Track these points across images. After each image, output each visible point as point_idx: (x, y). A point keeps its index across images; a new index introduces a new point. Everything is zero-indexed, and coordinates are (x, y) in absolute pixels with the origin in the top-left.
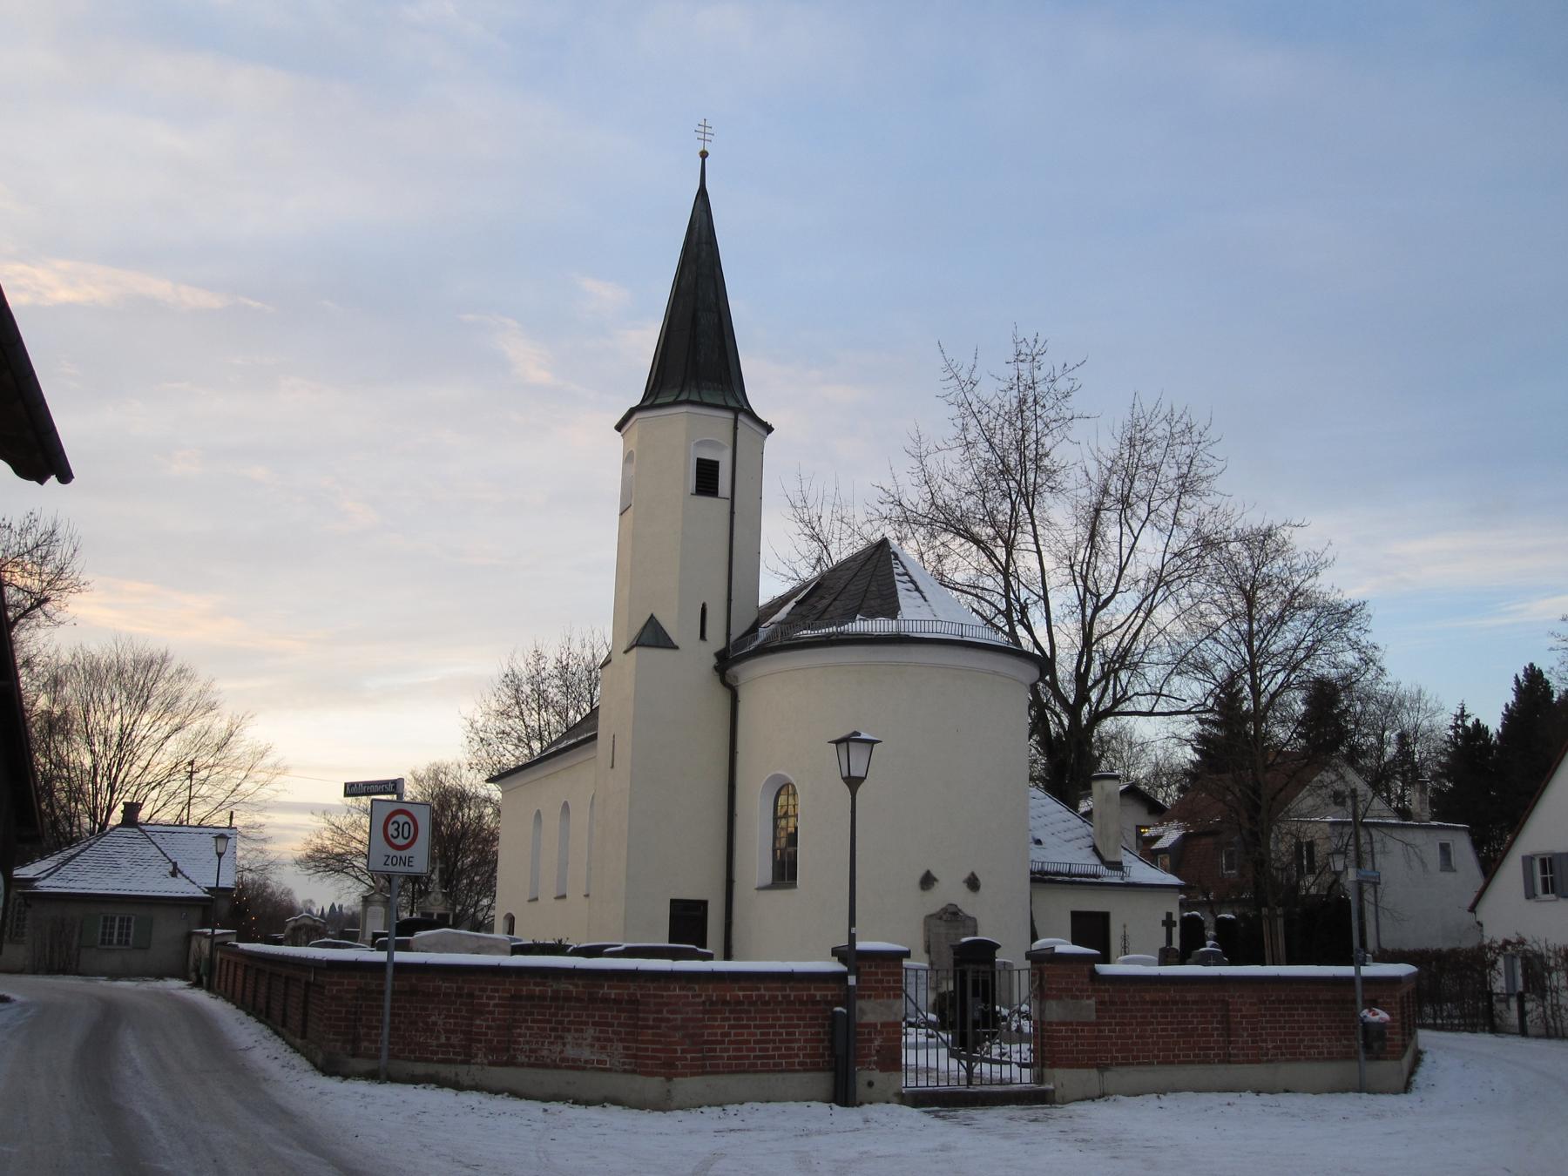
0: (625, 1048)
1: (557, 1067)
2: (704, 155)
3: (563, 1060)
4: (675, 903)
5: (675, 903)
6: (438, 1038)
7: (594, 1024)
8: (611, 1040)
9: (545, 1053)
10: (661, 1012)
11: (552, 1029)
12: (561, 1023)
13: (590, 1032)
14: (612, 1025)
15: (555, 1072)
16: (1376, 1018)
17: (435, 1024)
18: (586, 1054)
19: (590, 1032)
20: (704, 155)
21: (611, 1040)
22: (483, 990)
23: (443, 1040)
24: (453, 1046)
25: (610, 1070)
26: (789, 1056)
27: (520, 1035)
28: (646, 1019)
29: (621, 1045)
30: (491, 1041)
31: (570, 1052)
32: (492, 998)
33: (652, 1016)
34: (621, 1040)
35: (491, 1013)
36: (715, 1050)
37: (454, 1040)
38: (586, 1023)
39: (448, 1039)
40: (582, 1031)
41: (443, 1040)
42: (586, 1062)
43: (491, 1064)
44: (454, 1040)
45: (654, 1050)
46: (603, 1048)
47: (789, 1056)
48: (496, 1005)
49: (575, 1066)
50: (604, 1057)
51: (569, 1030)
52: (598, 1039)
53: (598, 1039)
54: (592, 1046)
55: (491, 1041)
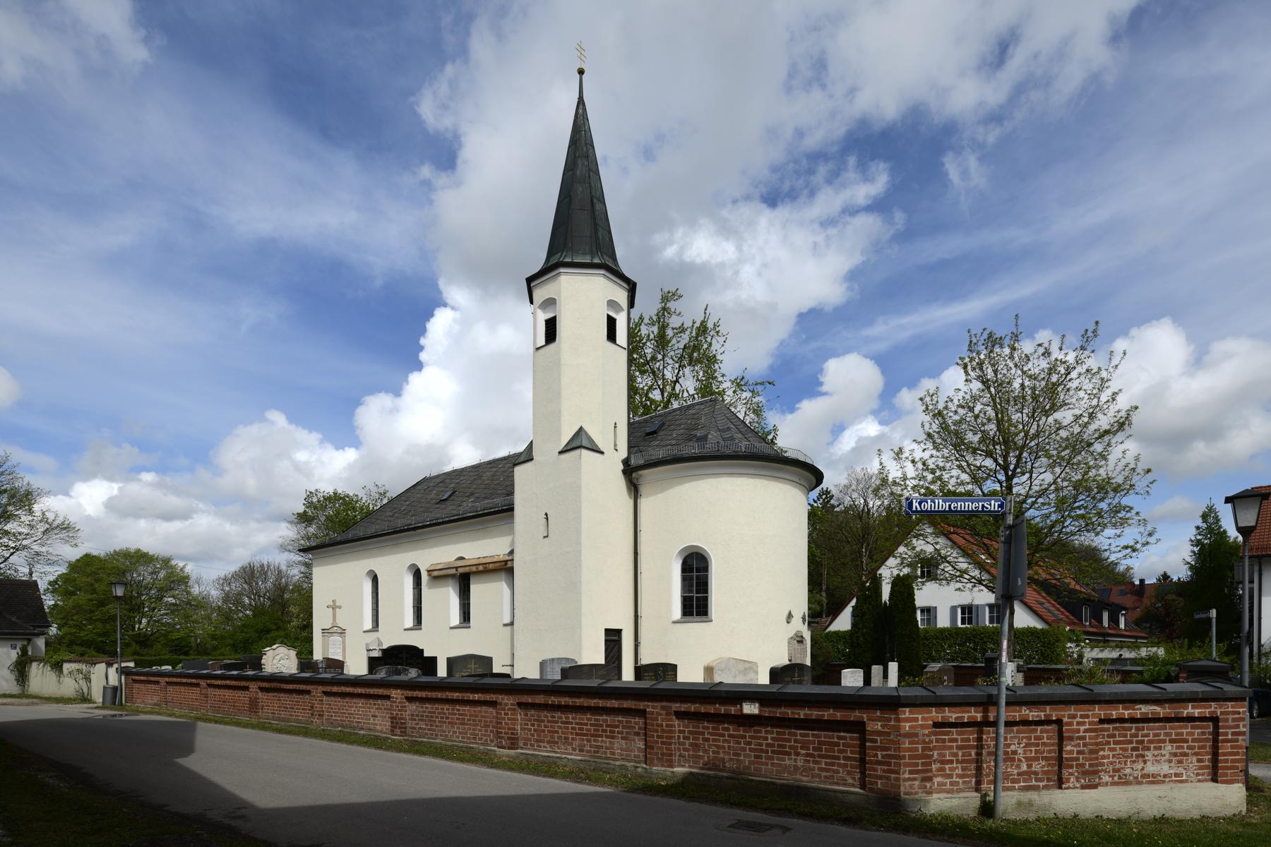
0: (1199, 761)
1: (1140, 783)
2: (581, 72)
3: (1144, 776)
4: (675, 666)
5: (675, 666)
6: (1018, 767)
7: (1172, 741)
8: (1186, 755)
9: (1128, 771)
10: (1238, 726)
11: (1134, 749)
12: (1142, 742)
13: (1168, 748)
14: (1186, 741)
15: (1137, 787)
16: (783, 710)
17: (1015, 752)
18: (1165, 768)
19: (1168, 748)
20: (581, 72)
21: (1186, 755)
22: (1074, 717)
23: (1024, 767)
24: (1036, 773)
25: (1186, 781)
26: (696, 733)
27: (1104, 757)
28: (1226, 734)
29: (1195, 759)
30: (1083, 765)
31: (1151, 768)
32: (1083, 724)
33: (1230, 731)
34: (1196, 754)
35: (1083, 738)
36: (962, 740)
37: (1036, 767)
38: (1164, 741)
39: (1029, 766)
40: (1160, 748)
41: (1024, 767)
42: (1165, 776)
43: (1083, 787)
44: (1036, 767)
45: (1233, 761)
46: (1180, 762)
47: (696, 733)
48: (1086, 731)
49: (1154, 780)
50: (1181, 770)
51: (1149, 749)
52: (1175, 755)
53: (1175, 755)
54: (1170, 761)
55: (1083, 765)
